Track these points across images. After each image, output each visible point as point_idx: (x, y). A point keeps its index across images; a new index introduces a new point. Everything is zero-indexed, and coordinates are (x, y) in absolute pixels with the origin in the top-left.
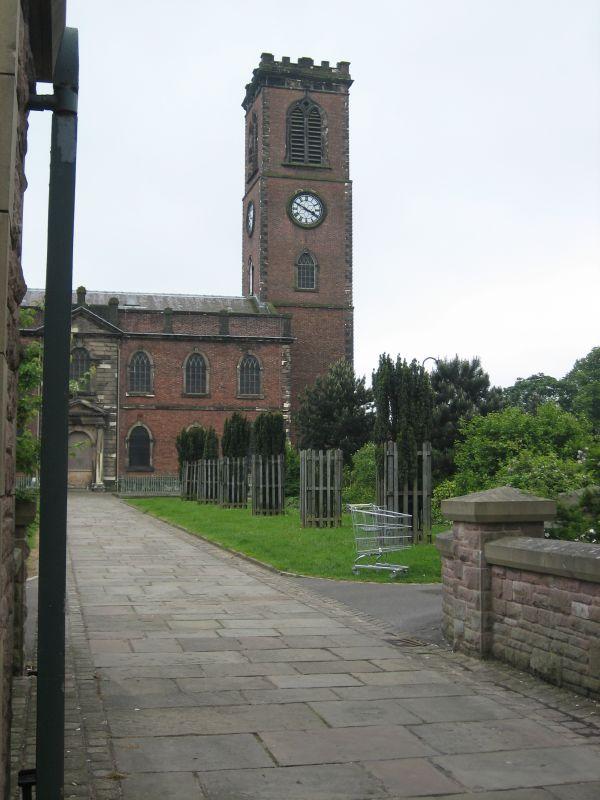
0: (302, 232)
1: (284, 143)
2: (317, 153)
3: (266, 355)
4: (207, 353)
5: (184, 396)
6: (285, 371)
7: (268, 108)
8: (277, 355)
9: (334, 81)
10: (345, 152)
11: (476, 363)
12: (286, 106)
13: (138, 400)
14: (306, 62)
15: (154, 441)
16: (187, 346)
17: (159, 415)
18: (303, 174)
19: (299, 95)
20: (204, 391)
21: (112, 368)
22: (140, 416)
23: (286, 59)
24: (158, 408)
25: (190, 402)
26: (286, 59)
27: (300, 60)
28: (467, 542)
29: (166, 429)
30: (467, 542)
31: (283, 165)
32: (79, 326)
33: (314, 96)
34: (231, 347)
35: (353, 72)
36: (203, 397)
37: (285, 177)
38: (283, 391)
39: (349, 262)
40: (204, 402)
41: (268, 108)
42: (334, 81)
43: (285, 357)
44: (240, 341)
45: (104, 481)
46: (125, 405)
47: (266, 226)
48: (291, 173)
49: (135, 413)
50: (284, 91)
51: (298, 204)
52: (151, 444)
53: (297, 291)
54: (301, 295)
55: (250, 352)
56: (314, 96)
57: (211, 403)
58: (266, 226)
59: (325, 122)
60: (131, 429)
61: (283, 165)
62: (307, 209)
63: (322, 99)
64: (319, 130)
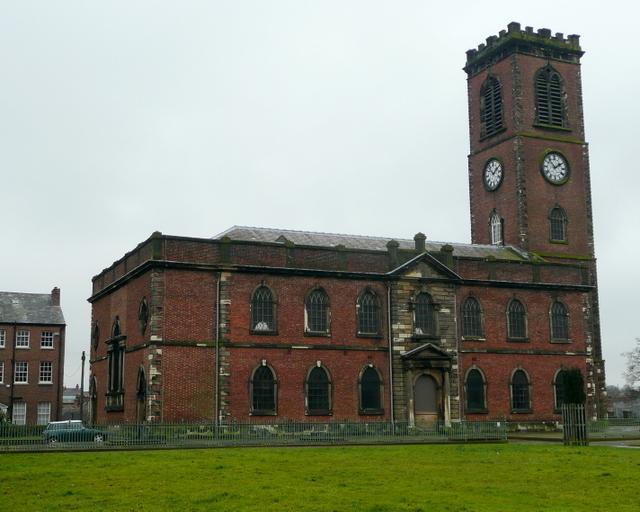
0: (552, 188)
1: (533, 105)
2: (559, 115)
3: (571, 301)
4: (525, 296)
5: (509, 341)
6: (586, 317)
7: (519, 73)
8: (579, 302)
9: (561, 53)
10: (581, 116)
11: (89, 300)
12: (533, 71)
13: (472, 345)
14: (545, 32)
15: (487, 383)
16: (508, 293)
17: (490, 360)
18: (551, 135)
19: (543, 63)
20: (523, 334)
21: (452, 312)
22: (474, 359)
23: (529, 29)
24: (488, 352)
25: (515, 347)
26: (529, 29)
27: (539, 30)
28: (264, 364)
29: (498, 371)
30: (264, 364)
31: (534, 126)
32: (422, 272)
33: (554, 64)
34: (543, 294)
35: (583, 44)
36: (524, 341)
37: (537, 138)
38: (586, 335)
39: (590, 217)
40: (524, 347)
41: (519, 73)
42: (561, 53)
43: (585, 305)
44: (550, 288)
45: (452, 423)
46: (464, 349)
47: (524, 181)
48: (540, 133)
49: (469, 356)
50: (531, 58)
51: (560, 165)
52: (485, 387)
53: (551, 242)
54: (555, 246)
55: (559, 299)
56: (554, 64)
57: (531, 347)
58: (524, 181)
59: (564, 88)
60: (468, 372)
61: (534, 126)
62: (555, 169)
63: (559, 66)
64: (559, 96)
